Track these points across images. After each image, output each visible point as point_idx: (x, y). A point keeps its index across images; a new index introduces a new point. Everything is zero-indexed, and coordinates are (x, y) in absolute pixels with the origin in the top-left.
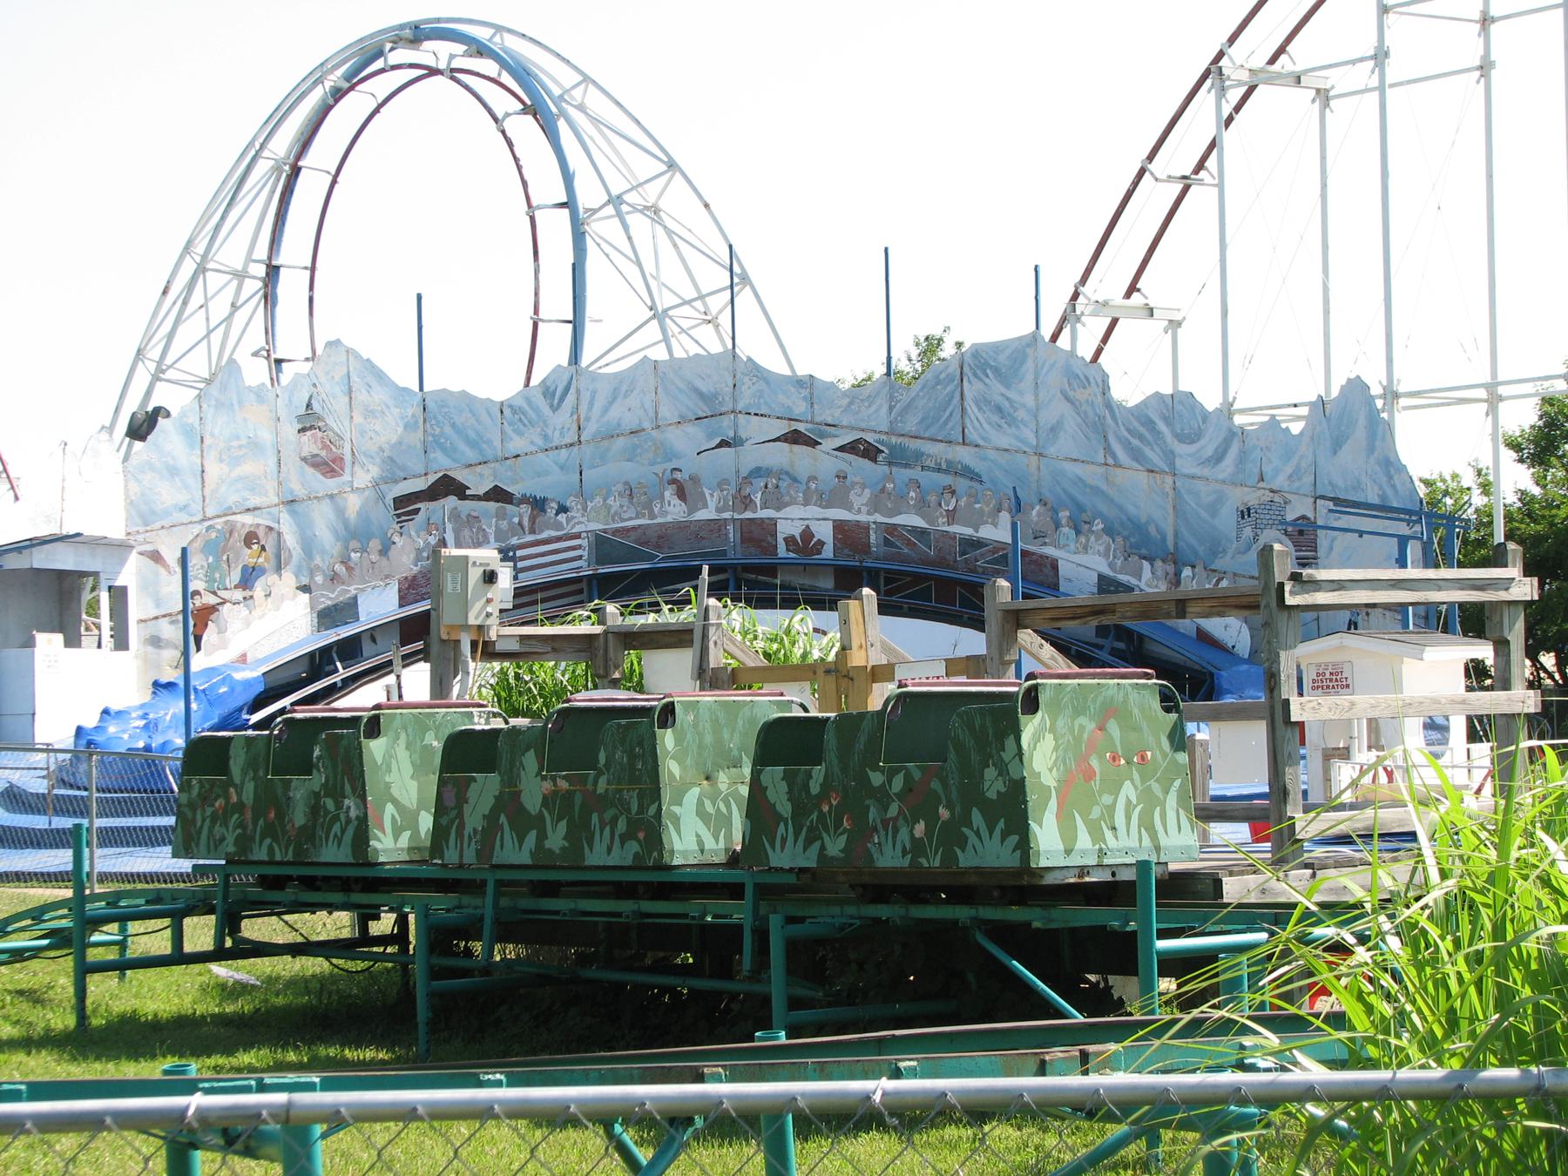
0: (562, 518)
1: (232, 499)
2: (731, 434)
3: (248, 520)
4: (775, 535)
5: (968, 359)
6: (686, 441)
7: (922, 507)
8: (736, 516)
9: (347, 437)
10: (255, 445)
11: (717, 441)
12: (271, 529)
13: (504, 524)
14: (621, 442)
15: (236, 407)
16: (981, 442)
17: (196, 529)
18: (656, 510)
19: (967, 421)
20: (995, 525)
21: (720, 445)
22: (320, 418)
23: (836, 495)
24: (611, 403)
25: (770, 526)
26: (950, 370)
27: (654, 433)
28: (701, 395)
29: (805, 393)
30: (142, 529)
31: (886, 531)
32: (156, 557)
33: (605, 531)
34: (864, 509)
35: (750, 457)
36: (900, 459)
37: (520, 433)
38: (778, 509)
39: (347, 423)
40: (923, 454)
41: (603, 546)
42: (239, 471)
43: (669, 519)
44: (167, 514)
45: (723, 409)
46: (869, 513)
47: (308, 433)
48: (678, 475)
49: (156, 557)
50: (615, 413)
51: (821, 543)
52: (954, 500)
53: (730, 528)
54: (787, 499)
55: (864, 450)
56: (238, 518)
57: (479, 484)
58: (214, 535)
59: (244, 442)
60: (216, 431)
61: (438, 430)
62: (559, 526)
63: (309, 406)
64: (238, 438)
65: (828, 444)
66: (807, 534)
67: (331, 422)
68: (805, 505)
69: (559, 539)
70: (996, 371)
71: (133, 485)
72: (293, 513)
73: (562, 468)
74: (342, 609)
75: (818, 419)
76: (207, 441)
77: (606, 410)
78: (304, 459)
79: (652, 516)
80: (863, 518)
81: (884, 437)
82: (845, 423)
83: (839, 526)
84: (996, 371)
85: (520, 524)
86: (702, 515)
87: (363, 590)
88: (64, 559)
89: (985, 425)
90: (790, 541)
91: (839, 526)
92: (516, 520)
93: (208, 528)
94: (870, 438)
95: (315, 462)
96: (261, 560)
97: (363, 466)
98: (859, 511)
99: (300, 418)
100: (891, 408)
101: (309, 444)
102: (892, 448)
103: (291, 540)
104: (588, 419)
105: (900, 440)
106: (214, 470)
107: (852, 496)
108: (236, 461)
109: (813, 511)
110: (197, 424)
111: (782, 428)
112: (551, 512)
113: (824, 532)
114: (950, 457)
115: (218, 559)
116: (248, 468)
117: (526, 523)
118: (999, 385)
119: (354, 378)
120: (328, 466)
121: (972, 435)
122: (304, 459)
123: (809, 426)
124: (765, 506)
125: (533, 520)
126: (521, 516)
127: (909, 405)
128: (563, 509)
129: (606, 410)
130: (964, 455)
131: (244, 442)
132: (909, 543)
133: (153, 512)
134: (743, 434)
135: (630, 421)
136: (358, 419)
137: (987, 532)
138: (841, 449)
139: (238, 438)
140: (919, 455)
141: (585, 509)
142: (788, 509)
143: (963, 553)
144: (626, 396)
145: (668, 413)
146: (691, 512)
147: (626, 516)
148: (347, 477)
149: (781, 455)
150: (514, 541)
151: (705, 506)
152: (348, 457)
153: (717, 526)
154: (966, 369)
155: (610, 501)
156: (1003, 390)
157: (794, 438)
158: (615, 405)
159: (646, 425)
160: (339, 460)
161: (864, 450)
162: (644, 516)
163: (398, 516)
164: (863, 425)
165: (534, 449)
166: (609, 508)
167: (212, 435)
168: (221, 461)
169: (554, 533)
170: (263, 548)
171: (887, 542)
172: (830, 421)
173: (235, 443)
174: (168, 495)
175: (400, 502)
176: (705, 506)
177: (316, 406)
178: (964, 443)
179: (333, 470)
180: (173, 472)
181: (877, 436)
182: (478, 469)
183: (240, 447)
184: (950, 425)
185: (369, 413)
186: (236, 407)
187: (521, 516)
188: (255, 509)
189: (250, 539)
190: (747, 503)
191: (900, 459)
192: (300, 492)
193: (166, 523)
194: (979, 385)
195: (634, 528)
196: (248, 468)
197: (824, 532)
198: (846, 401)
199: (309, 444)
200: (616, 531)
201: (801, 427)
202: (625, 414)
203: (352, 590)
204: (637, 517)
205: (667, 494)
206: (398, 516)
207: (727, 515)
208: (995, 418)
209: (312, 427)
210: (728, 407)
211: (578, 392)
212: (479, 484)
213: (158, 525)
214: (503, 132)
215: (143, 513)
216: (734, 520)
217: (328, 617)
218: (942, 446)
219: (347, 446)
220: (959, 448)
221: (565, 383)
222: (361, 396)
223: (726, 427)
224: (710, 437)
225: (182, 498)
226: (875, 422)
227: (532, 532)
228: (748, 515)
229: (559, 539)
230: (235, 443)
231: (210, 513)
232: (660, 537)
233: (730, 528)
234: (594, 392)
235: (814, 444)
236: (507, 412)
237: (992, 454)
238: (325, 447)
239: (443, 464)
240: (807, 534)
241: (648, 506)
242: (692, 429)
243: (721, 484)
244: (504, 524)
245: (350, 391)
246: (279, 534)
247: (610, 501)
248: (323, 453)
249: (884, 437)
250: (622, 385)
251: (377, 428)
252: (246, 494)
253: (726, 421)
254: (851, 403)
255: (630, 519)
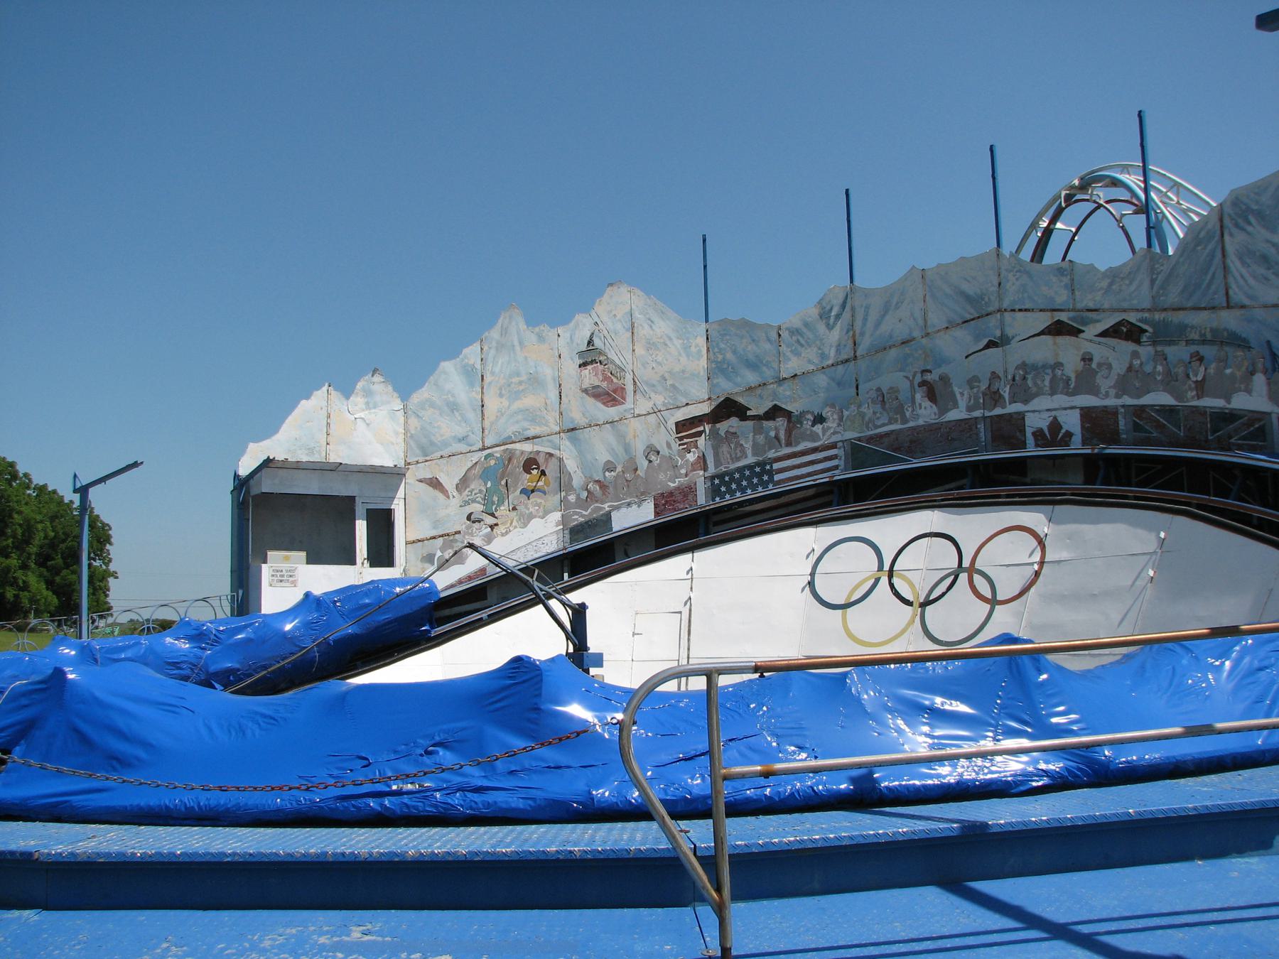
0: (818, 428)
1: (510, 430)
2: (998, 333)
3: (527, 447)
4: (1023, 431)
5: (1228, 210)
6: (954, 346)
7: (1170, 382)
8: (988, 414)
9: (629, 368)
10: (535, 381)
11: (985, 342)
12: (551, 455)
13: (761, 439)
14: (893, 353)
15: (518, 348)
16: (1246, 302)
17: (475, 457)
18: (908, 414)
19: (1231, 280)
20: (1249, 391)
21: (987, 346)
22: (601, 353)
23: (1086, 380)
24: (883, 316)
25: (1017, 421)
26: (1210, 226)
27: (924, 341)
28: (968, 298)
29: (1066, 280)
30: (421, 459)
31: (1135, 414)
32: (435, 484)
33: (859, 439)
34: (1113, 392)
35: (1018, 353)
36: (1165, 335)
37: (798, 354)
38: (1026, 402)
39: (629, 356)
40: (1186, 326)
41: (857, 454)
42: (518, 405)
43: (921, 422)
44: (446, 444)
45: (991, 309)
46: (1118, 396)
47: (589, 367)
48: (928, 377)
49: (435, 484)
50: (885, 328)
51: (1069, 435)
52: (1202, 369)
53: (981, 426)
54: (1034, 390)
55: (1126, 332)
56: (517, 446)
57: (758, 406)
58: (492, 463)
59: (524, 378)
60: (497, 370)
61: (720, 357)
62: (814, 437)
63: (590, 342)
64: (518, 375)
65: (1091, 331)
66: (1055, 425)
67: (612, 355)
68: (1052, 395)
69: (815, 450)
70: (1259, 215)
71: (413, 422)
72: (574, 441)
73: (839, 384)
74: (596, 525)
75: (1079, 306)
76: (488, 379)
77: (878, 325)
78: (585, 391)
79: (905, 421)
80: (1111, 402)
81: (1146, 315)
82: (1106, 306)
83: (1087, 413)
84: (1259, 215)
85: (777, 437)
86: (953, 415)
87: (618, 508)
88: (338, 488)
89: (1251, 281)
90: (1038, 434)
91: (1087, 413)
92: (772, 434)
93: (486, 458)
94: (1132, 318)
95: (596, 393)
96: (540, 483)
97: (644, 394)
98: (1107, 395)
99: (581, 354)
100: (1153, 282)
101: (590, 377)
102: (1153, 324)
103: (571, 465)
104: (862, 334)
105: (1163, 315)
106: (493, 404)
107: (1099, 380)
108: (516, 395)
109: (1061, 400)
110: (478, 366)
111: (1044, 320)
112: (807, 425)
113: (1071, 422)
114: (1215, 325)
115: (496, 483)
116: (529, 401)
117: (782, 435)
118: (1263, 231)
119: (637, 315)
120: (610, 396)
121: (1238, 295)
122: (585, 391)
123: (1071, 314)
124: (1013, 401)
125: (789, 432)
126: (776, 429)
127: (1170, 275)
128: (819, 419)
129: (878, 325)
130: (1229, 320)
131: (524, 378)
132: (1159, 426)
133: (432, 444)
134: (1009, 332)
135: (901, 332)
136: (640, 351)
137: (1240, 402)
138: (1104, 334)
139: (518, 375)
140: (1183, 328)
141: (841, 419)
142: (1036, 401)
143: (1214, 432)
144: (897, 307)
145: (937, 319)
146: (943, 412)
147: (879, 423)
148: (629, 404)
149: (1044, 350)
150: (772, 454)
151: (956, 406)
152: (630, 388)
153: (966, 426)
154: (1227, 221)
155: (864, 409)
156: (1268, 235)
157: (1058, 329)
158: (887, 317)
159: (916, 334)
160: (621, 390)
161: (1126, 332)
162: (896, 421)
163: (681, 439)
164: (1125, 305)
165: (811, 367)
166: (862, 415)
167: (493, 373)
168: (501, 395)
169: (810, 445)
170: (543, 473)
171: (1137, 427)
172: (1091, 305)
173: (516, 380)
174: (447, 428)
175: (681, 426)
176: (956, 406)
177: (598, 343)
178: (1228, 307)
179: (614, 399)
180: (453, 407)
181: (1140, 315)
182: (759, 391)
183: (520, 383)
184: (1213, 287)
185: (650, 346)
186: (518, 348)
187: (776, 429)
188: (534, 438)
189: (530, 464)
190: (994, 397)
191: (1165, 335)
192: (578, 418)
193: (445, 452)
194: (1240, 237)
195: (887, 434)
196: (529, 401)
197: (1071, 422)
198: (1105, 284)
199: (590, 377)
200: (870, 439)
201: (1063, 317)
202: (895, 326)
203: (606, 507)
204: (890, 423)
205: (918, 396)
206: (681, 439)
207: (978, 413)
208: (1261, 271)
209: (593, 362)
210: (996, 306)
211: (853, 309)
212: (758, 406)
213: (438, 454)
214: (1123, 228)
215: (424, 447)
216: (984, 418)
217: (576, 532)
218: (1204, 315)
219: (629, 377)
220: (1224, 314)
221: (841, 301)
222: (643, 331)
223: (992, 327)
224: (977, 338)
225: (460, 430)
226: (1136, 300)
227: (789, 444)
228: (998, 411)
229: (815, 450)
230: (516, 380)
231: (488, 443)
232: (911, 442)
233: (981, 426)
234: (867, 308)
235: (1076, 332)
236: (785, 334)
237: (1259, 313)
238: (605, 378)
239: (727, 388)
240: (1055, 425)
241: (900, 410)
242: (959, 333)
243: (972, 382)
244: (761, 439)
245: (633, 327)
246: (560, 460)
247: (864, 409)
248: (604, 385)
249: (1146, 315)
250: (891, 299)
251: (660, 359)
252: (526, 424)
253: (993, 321)
254: (1111, 284)
255: (884, 425)
